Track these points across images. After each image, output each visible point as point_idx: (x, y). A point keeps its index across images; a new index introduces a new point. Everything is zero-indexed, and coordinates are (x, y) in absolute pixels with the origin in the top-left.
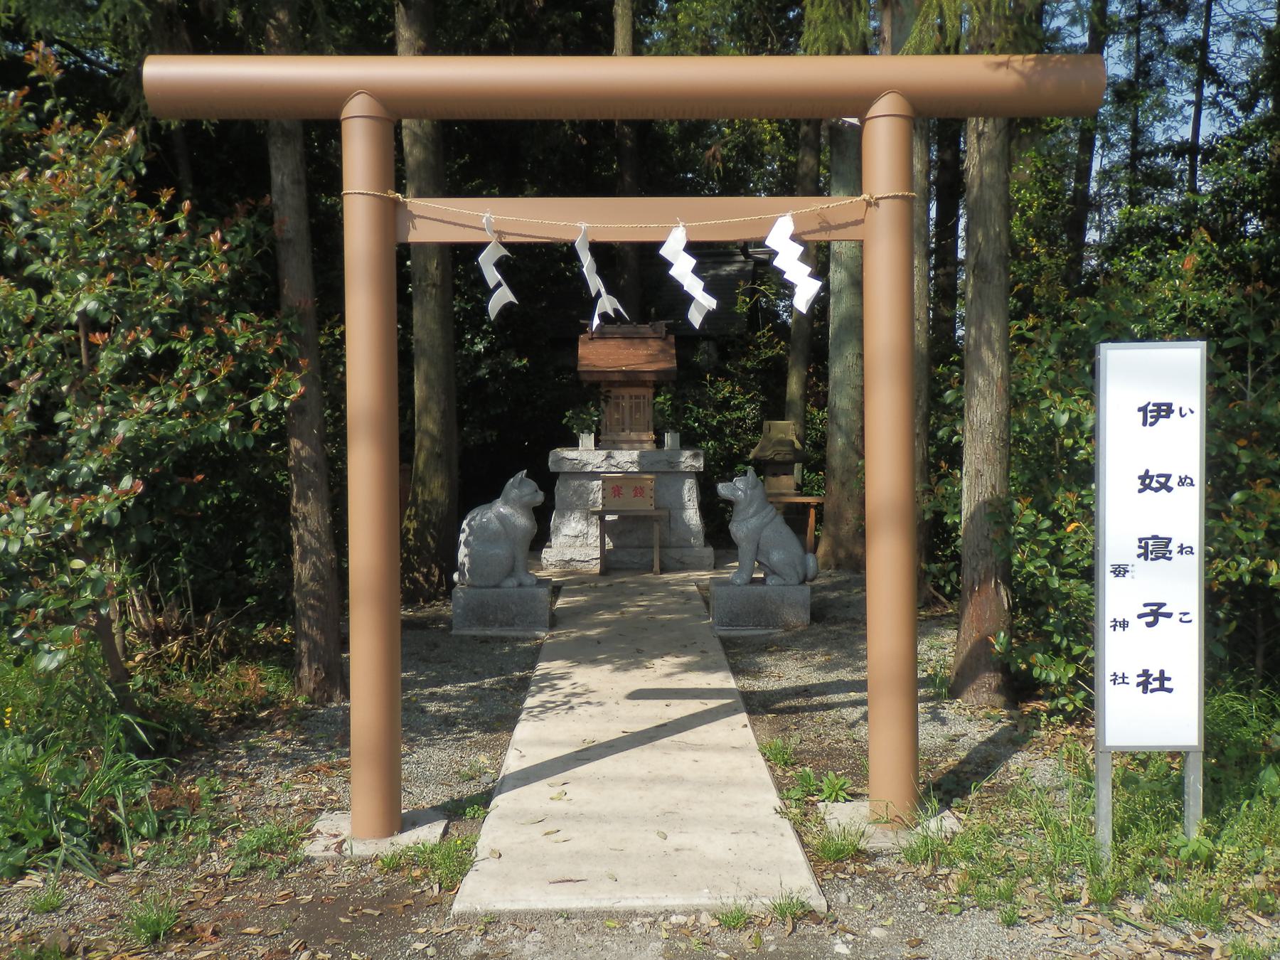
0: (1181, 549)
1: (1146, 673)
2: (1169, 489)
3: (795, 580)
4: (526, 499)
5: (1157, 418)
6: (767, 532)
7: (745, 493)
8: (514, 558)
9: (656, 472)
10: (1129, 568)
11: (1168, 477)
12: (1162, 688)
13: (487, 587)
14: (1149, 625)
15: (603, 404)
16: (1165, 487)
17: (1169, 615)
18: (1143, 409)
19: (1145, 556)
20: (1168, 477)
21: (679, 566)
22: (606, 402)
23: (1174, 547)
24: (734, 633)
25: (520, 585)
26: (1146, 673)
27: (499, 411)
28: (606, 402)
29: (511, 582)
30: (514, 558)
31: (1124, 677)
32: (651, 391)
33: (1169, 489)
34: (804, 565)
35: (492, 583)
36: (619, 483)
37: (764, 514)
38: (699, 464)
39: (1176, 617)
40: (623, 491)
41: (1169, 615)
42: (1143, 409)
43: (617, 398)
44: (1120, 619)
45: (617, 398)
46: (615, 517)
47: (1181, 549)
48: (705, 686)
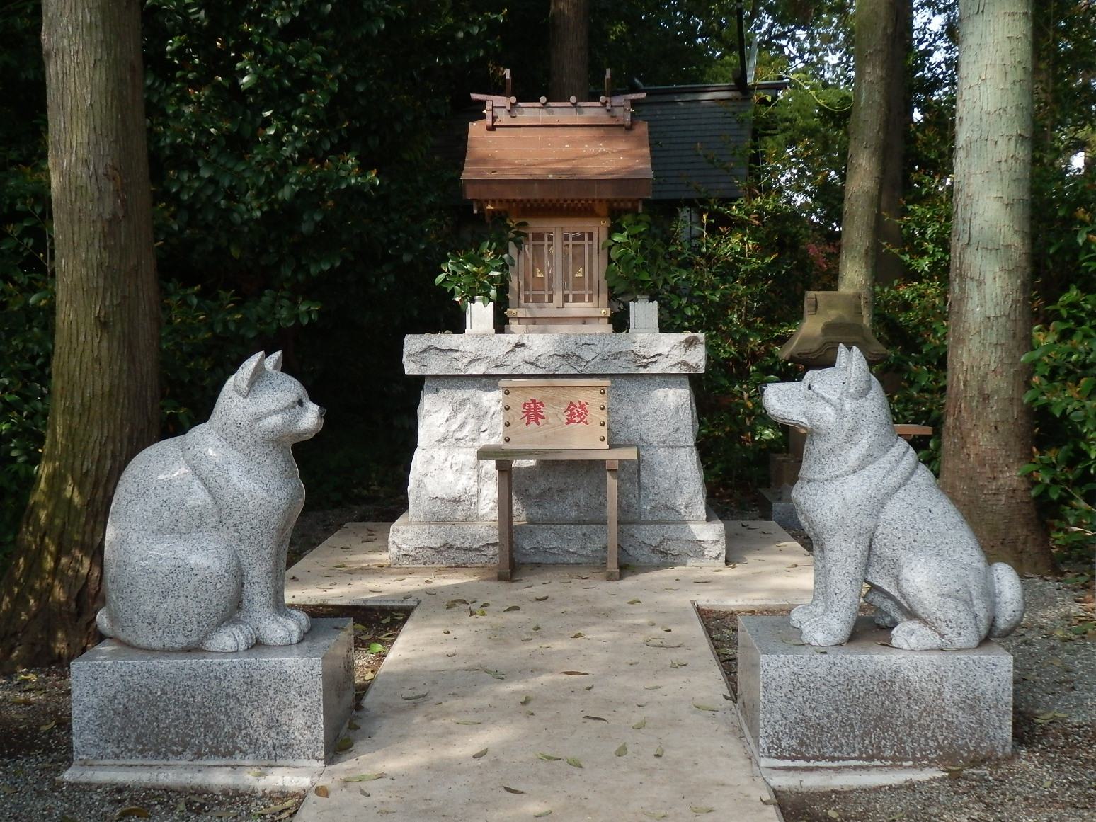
3: (969, 637)
4: (274, 421)
6: (893, 510)
7: (839, 410)
8: (239, 577)
9: (611, 376)
13: (167, 651)
15: (513, 249)
21: (656, 559)
22: (519, 244)
24: (813, 782)
25: (257, 644)
27: (326, 267)
28: (519, 244)
29: (227, 639)
30: (239, 577)
32: (605, 223)
34: (990, 595)
35: (181, 640)
36: (537, 396)
37: (886, 460)
38: (698, 358)
40: (546, 411)
43: (539, 237)
45: (539, 237)
46: (532, 463)
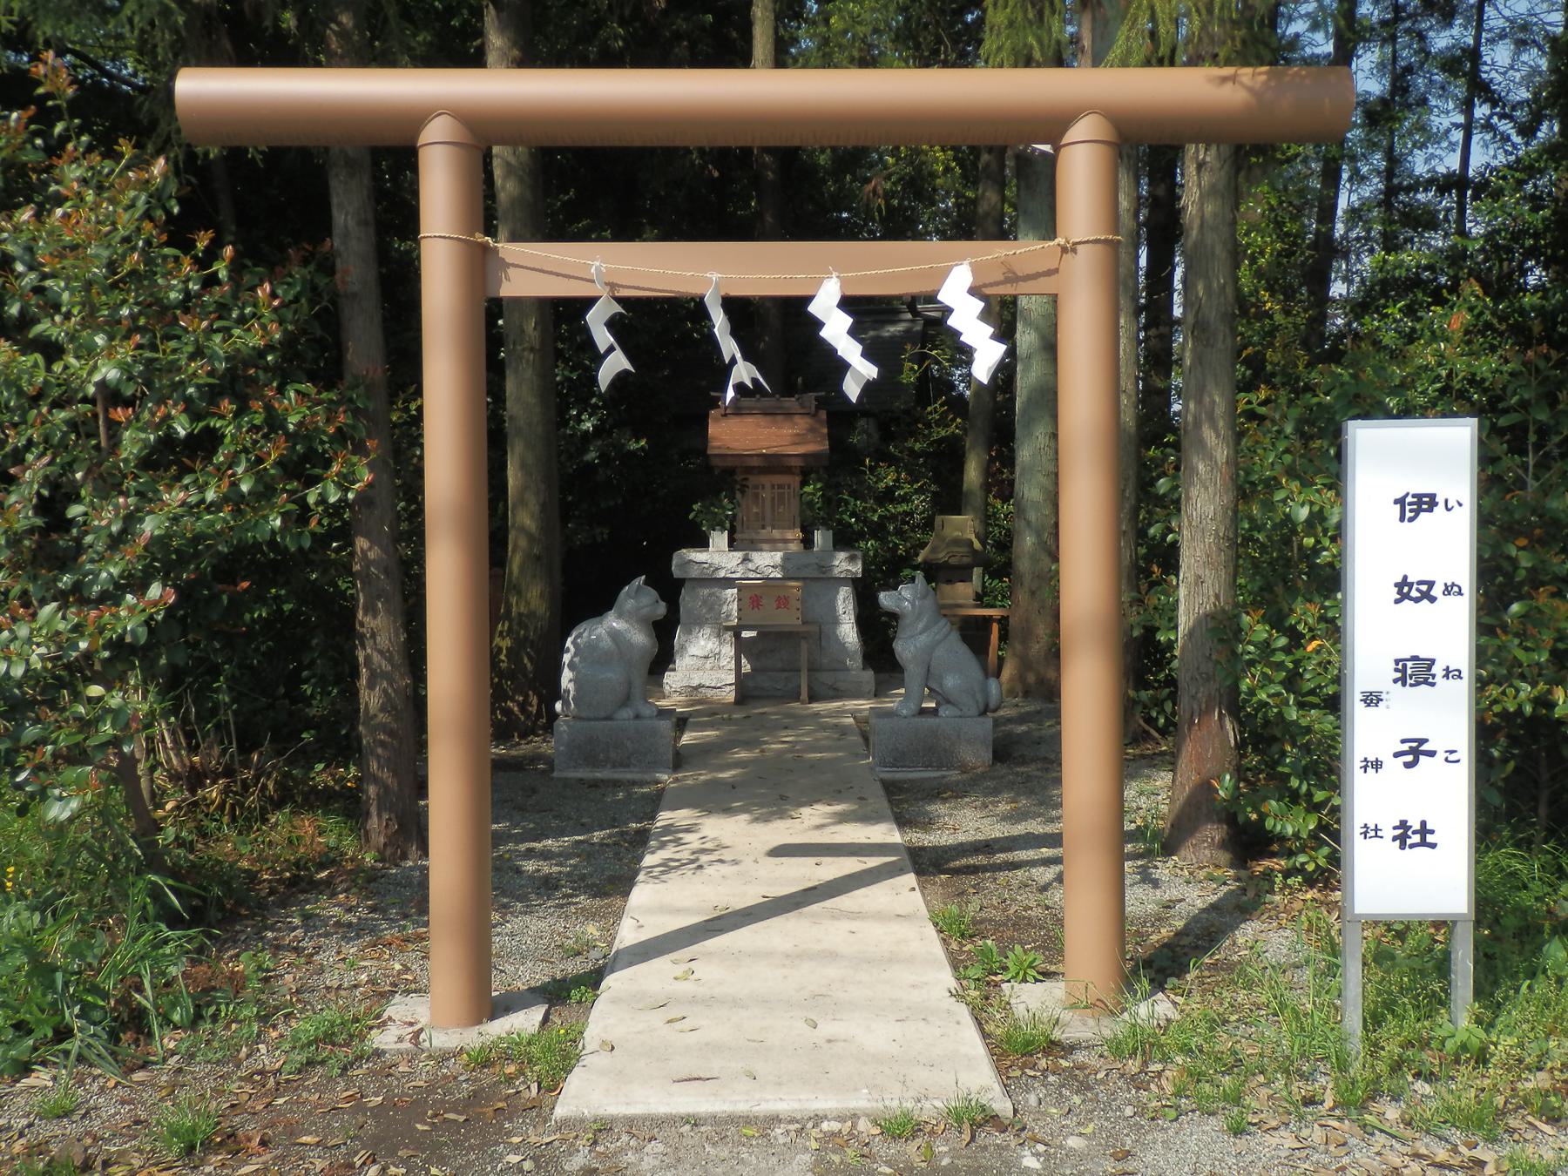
0: (1447, 673)
1: (1403, 825)
2: (1433, 600)
3: (974, 711)
4: (645, 611)
5: (1417, 512)
6: (939, 652)
7: (913, 604)
8: (630, 684)
9: (804, 579)
10: (1383, 696)
11: (1431, 584)
12: (1423, 843)
13: (596, 719)
14: (1408, 765)
15: (738, 495)
16: (1428, 596)
17: (1432, 754)
18: (1401, 501)
19: (1403, 681)
20: (1431, 584)
21: (831, 693)
22: (743, 492)
23: (1438, 670)
24: (899, 776)
25: (637, 717)
26: (1403, 825)
27: (612, 503)
28: (743, 492)
29: (626, 713)
30: (630, 684)
31: (1376, 829)
32: (798, 479)
33: (1433, 600)
34: (985, 692)
35: (603, 714)
36: (758, 592)
37: (935, 629)
38: (857, 568)
39: (1441, 756)
40: (764, 601)
41: (1432, 754)
42: (1401, 501)
43: (756, 487)
44: (1372, 758)
45: (756, 487)
46: (753, 634)
47: (1447, 673)
48: (863, 840)
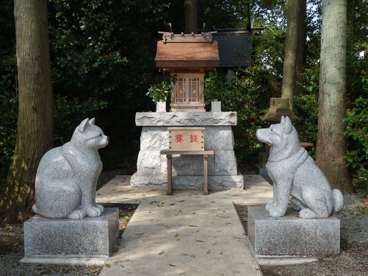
3: (325, 214)
4: (92, 141)
6: (300, 171)
7: (282, 138)
8: (80, 194)
9: (205, 126)
13: (56, 219)
15: (172, 84)
21: (220, 188)
22: (174, 82)
24: (273, 262)
25: (86, 216)
27: (109, 90)
28: (174, 82)
29: (76, 215)
30: (80, 194)
32: (203, 75)
34: (332, 200)
35: (61, 215)
36: (180, 133)
37: (298, 155)
38: (234, 120)
40: (183, 138)
43: (181, 79)
45: (181, 79)
46: (179, 155)
